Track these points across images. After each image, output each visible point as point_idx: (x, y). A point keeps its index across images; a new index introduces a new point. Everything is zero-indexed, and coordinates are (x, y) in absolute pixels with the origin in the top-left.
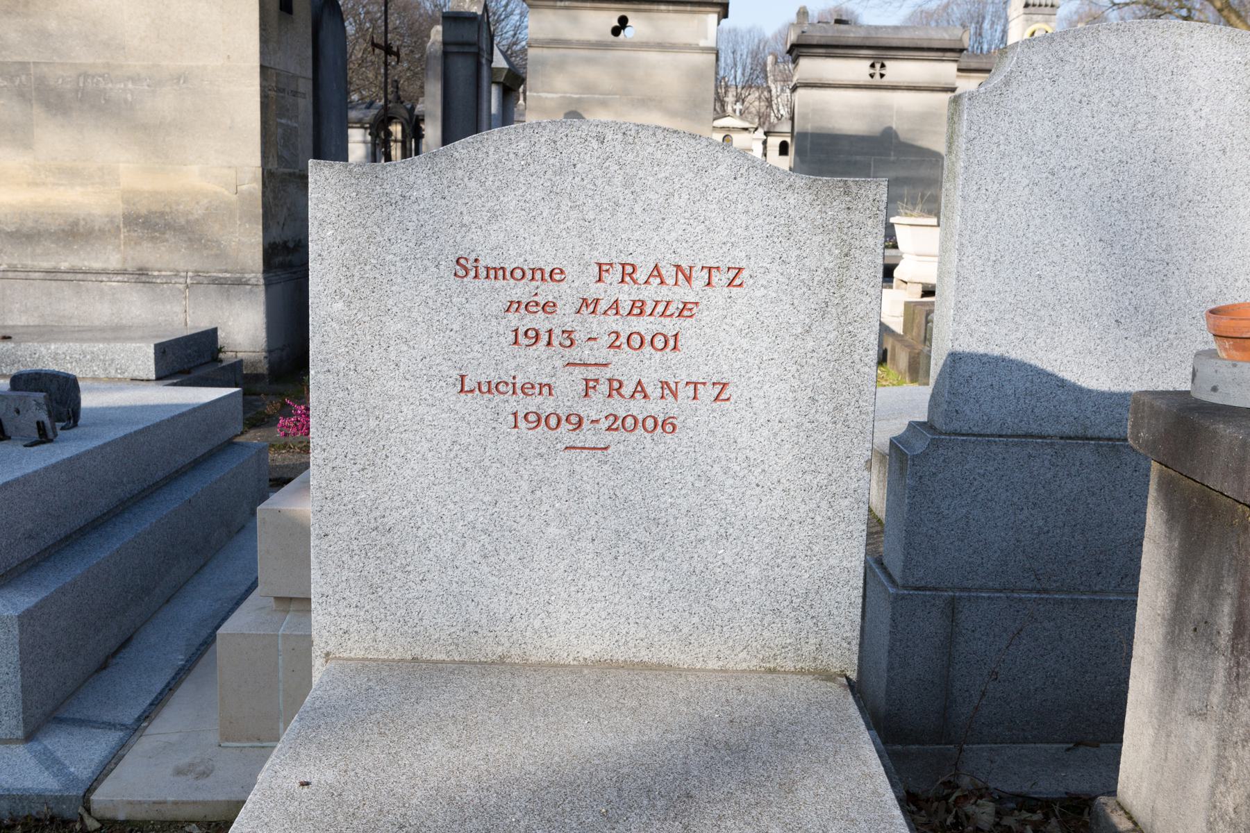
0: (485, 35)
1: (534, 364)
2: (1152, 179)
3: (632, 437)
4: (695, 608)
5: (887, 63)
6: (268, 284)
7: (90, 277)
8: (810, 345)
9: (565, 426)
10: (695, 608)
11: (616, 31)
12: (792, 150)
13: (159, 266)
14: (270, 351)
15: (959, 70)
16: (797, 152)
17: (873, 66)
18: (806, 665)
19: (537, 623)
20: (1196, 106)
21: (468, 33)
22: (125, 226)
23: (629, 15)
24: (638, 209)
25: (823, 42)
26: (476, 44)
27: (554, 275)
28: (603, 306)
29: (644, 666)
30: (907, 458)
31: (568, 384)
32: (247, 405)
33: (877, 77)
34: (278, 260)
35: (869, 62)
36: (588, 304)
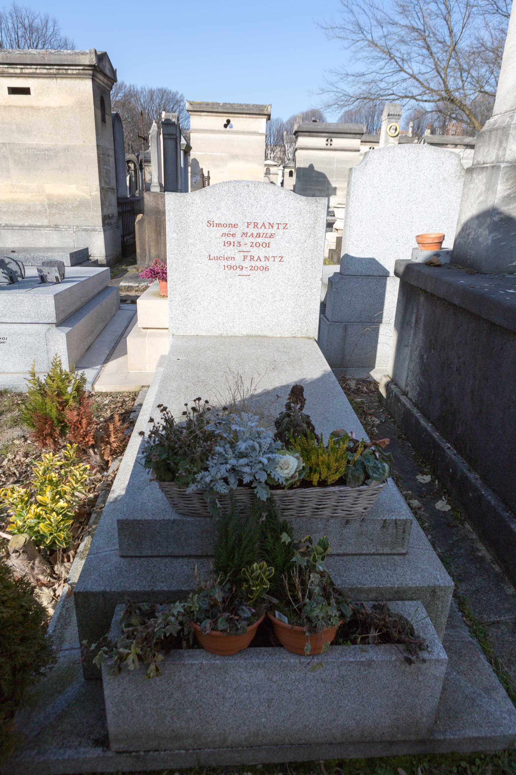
0: (178, 130)
1: (230, 251)
2: (409, 195)
3: (257, 272)
4: (274, 320)
5: (333, 139)
6: (104, 231)
7: (37, 228)
8: (306, 246)
9: (238, 269)
10: (274, 320)
11: (226, 126)
12: (294, 175)
13: (63, 224)
14: (106, 256)
15: (362, 142)
16: (297, 177)
17: (327, 140)
18: (304, 335)
19: (231, 325)
20: (423, 172)
21: (172, 130)
22: (49, 208)
23: (231, 119)
24: (258, 207)
25: (308, 130)
26: (176, 135)
27: (235, 226)
28: (249, 235)
29: (259, 336)
30: (333, 283)
31: (239, 257)
32: (111, 272)
33: (329, 145)
34: (107, 222)
35: (326, 139)
36: (245, 234)
